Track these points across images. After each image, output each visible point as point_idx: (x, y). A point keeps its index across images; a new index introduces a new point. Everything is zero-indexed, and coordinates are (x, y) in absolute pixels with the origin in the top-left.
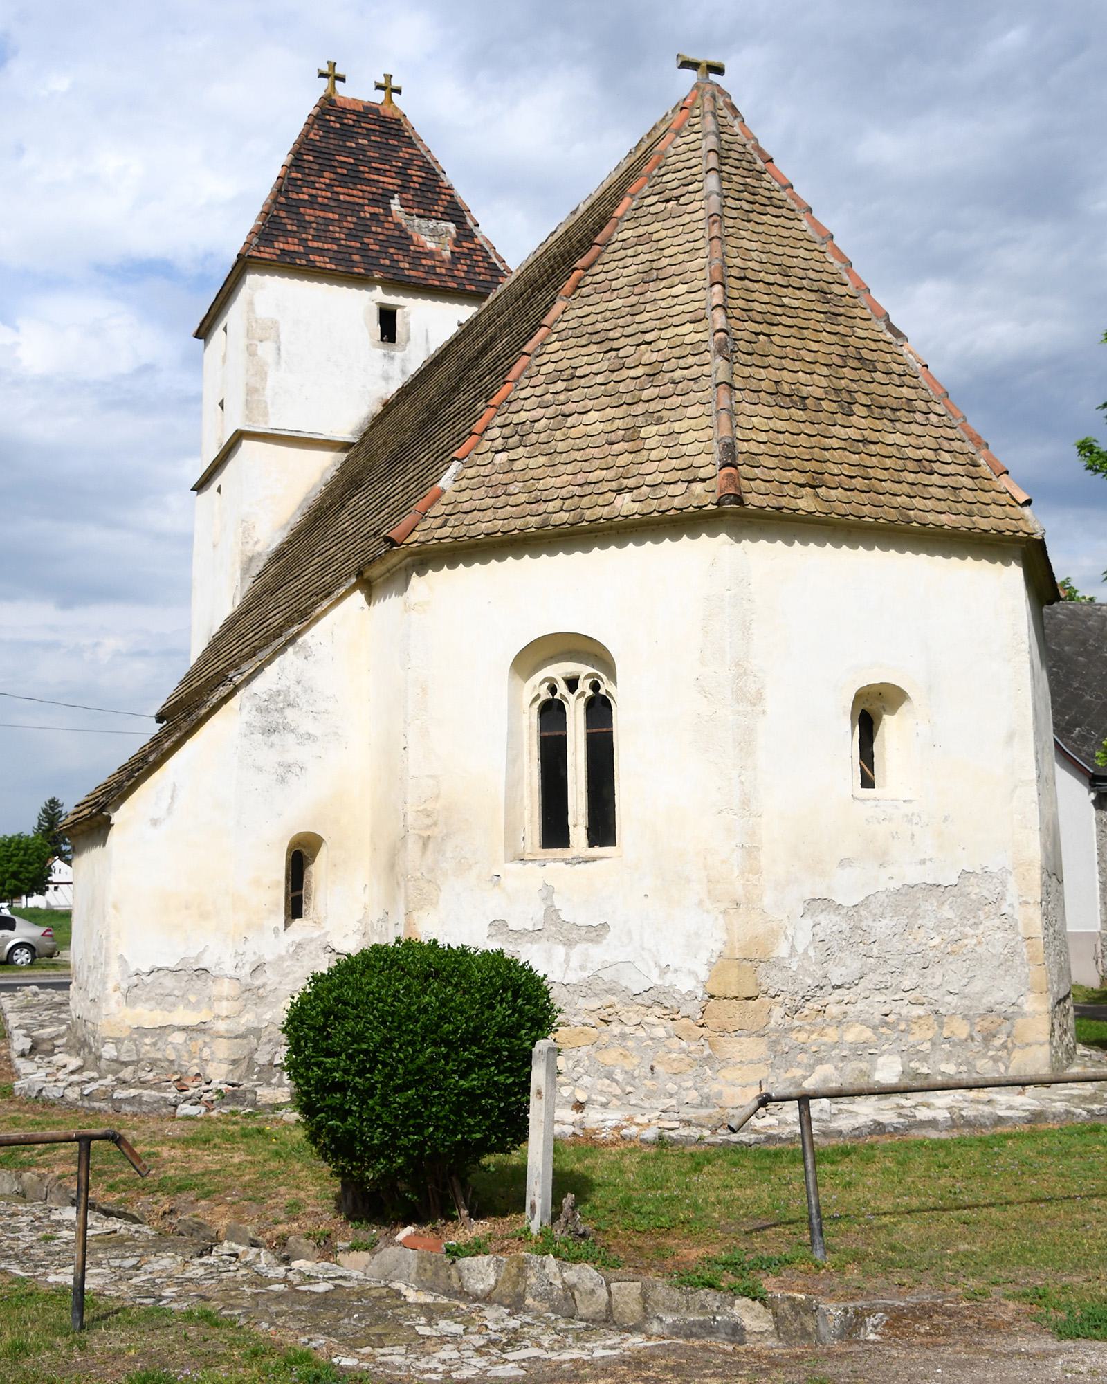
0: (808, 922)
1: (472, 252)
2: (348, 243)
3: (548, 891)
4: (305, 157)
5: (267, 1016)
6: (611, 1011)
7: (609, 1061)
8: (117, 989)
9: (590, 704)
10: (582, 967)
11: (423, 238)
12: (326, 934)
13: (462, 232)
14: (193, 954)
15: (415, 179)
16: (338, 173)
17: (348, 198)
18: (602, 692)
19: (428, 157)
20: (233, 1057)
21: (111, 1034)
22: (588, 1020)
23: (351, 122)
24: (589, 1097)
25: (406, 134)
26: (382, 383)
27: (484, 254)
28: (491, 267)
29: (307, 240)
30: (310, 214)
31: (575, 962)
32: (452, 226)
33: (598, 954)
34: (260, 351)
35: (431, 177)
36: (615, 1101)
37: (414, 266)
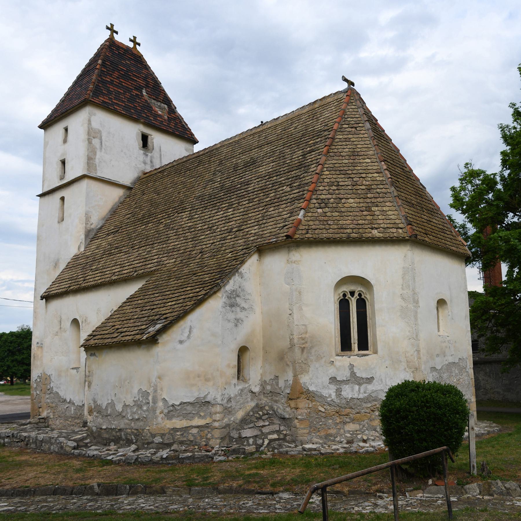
0: (431, 375)
3: (352, 366)
4: (107, 63)
5: (232, 419)
6: (375, 407)
7: (374, 424)
8: (161, 412)
9: (358, 301)
10: (365, 392)
11: (157, 109)
12: (250, 385)
14: (202, 395)
15: (151, 84)
16: (120, 73)
17: (126, 85)
18: (363, 297)
20: (221, 436)
21: (159, 432)
22: (367, 411)
23: (122, 53)
24: (368, 438)
26: (143, 165)
31: (362, 391)
32: (166, 106)
33: (371, 387)
34: (93, 142)
36: (377, 438)
37: (156, 119)
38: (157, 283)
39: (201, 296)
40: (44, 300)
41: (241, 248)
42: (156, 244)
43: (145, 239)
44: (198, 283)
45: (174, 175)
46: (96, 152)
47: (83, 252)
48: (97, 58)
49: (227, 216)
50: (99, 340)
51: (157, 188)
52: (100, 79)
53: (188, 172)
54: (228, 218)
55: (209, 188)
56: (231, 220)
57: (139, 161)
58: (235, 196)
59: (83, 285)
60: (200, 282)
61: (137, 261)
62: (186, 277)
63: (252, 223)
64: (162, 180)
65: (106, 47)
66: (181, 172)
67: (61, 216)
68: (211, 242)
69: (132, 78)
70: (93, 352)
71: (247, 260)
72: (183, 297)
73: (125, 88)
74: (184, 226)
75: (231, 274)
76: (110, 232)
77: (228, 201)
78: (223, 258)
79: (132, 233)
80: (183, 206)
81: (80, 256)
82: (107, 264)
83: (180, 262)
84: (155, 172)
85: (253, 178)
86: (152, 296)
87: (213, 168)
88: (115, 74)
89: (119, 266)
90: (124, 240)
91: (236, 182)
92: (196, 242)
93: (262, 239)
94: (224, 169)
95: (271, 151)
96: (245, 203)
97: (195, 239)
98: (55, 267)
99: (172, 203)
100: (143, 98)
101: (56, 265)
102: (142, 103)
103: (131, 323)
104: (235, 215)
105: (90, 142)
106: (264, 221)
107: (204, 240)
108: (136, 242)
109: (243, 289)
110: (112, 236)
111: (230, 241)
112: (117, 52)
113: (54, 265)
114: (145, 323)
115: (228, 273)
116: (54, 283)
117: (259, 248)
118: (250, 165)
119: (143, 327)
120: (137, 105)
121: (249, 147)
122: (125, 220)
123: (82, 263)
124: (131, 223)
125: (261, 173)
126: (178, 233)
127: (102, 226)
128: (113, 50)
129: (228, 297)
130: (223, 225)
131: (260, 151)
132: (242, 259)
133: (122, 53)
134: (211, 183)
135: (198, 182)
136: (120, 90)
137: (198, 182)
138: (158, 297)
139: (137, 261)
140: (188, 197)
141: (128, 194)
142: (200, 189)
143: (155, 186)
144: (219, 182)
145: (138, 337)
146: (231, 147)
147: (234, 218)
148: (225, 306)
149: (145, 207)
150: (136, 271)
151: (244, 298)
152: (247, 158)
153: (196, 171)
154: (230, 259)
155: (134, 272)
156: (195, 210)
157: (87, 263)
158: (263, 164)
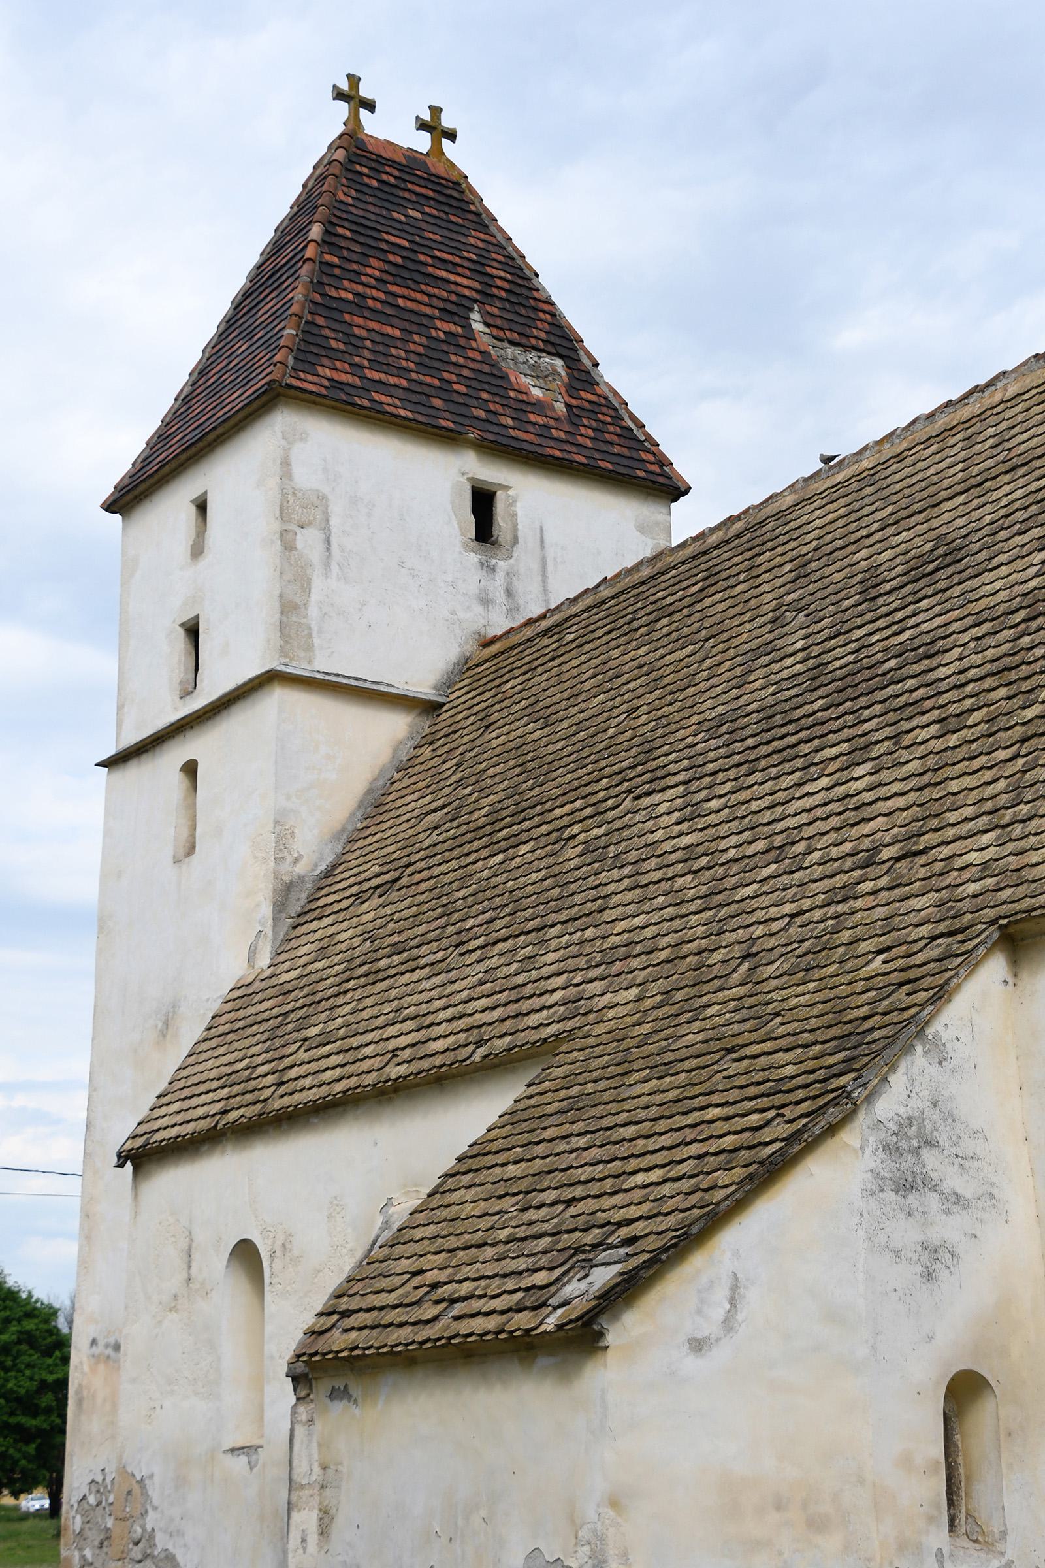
1: (596, 409)
2: (422, 378)
4: (340, 231)
13: (576, 374)
15: (499, 282)
16: (390, 262)
19: (510, 249)
23: (392, 180)
25: (472, 208)
26: (478, 609)
27: (612, 413)
28: (626, 433)
29: (362, 367)
30: (360, 325)
32: (559, 363)
34: (300, 545)
35: (520, 281)
38: (574, 1091)
39: (778, 1145)
40: (129, 1165)
41: (924, 931)
42: (552, 926)
43: (508, 910)
44: (753, 1091)
45: (605, 639)
46: (309, 580)
47: (268, 973)
48: (305, 220)
49: (848, 796)
50: (366, 1332)
51: (542, 696)
52: (317, 298)
53: (665, 621)
54: (852, 802)
55: (757, 684)
56: (867, 812)
57: (465, 594)
58: (878, 708)
59: (277, 1104)
60: (759, 1084)
61: (484, 1002)
62: (694, 1062)
63: (967, 820)
64: (556, 662)
65: (335, 169)
66: (636, 624)
67: (185, 833)
68: (788, 908)
69: (430, 275)
70: (339, 1383)
71: (959, 986)
72: (695, 1149)
73: (407, 316)
74: (667, 846)
75: (895, 1048)
76: (366, 885)
77: (846, 733)
78: (849, 977)
79: (455, 886)
80: (654, 764)
81: (258, 986)
82: (365, 1014)
83: (659, 998)
84: (529, 632)
85: (956, 626)
86: (562, 1146)
87: (770, 597)
88: (369, 271)
89: (410, 1025)
90: (425, 917)
91: (876, 648)
92: (723, 912)
93: (1022, 890)
94: (819, 595)
95: (1031, 499)
96: (924, 734)
97: (717, 899)
98: (164, 1036)
99: (606, 753)
100: (474, 344)
101: (167, 1026)
102: (471, 365)
103: (485, 1262)
104: (883, 792)
105: (288, 546)
106: (1024, 809)
107: (754, 904)
108: (470, 923)
109: (951, 1114)
110: (376, 901)
111: (870, 901)
112: (375, 183)
113: (160, 1025)
114: (544, 1261)
115: (881, 1044)
116: (164, 1100)
117: (1011, 930)
118: (937, 570)
119: (541, 1278)
120: (454, 378)
121: (925, 494)
122: (422, 836)
123: (265, 1015)
124: (446, 846)
125: (992, 601)
126: (644, 880)
127: (335, 866)
128: (361, 174)
129: (887, 1149)
130: (833, 835)
131: (975, 503)
132: (938, 979)
133: (392, 180)
134: (765, 660)
135: (708, 662)
136: (389, 330)
137: (708, 662)
138: (585, 1149)
139: (484, 1002)
140: (673, 727)
141: (427, 731)
142: (719, 690)
143: (534, 691)
144: (800, 656)
145: (523, 1320)
146: (843, 501)
147: (881, 804)
148: (875, 1188)
149: (497, 779)
150: (479, 1043)
151: (954, 1150)
152: (918, 541)
153: (698, 616)
154: (879, 982)
155: (472, 1047)
156: (707, 780)
157: (286, 1014)
158: (995, 562)
